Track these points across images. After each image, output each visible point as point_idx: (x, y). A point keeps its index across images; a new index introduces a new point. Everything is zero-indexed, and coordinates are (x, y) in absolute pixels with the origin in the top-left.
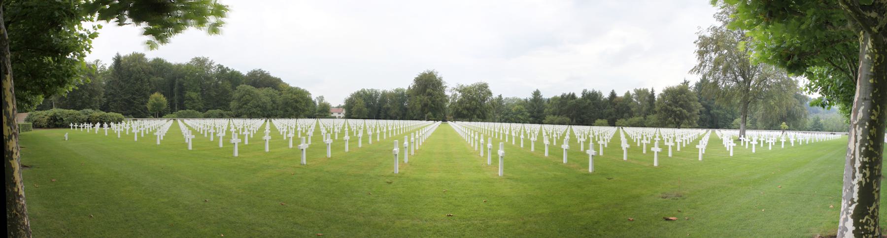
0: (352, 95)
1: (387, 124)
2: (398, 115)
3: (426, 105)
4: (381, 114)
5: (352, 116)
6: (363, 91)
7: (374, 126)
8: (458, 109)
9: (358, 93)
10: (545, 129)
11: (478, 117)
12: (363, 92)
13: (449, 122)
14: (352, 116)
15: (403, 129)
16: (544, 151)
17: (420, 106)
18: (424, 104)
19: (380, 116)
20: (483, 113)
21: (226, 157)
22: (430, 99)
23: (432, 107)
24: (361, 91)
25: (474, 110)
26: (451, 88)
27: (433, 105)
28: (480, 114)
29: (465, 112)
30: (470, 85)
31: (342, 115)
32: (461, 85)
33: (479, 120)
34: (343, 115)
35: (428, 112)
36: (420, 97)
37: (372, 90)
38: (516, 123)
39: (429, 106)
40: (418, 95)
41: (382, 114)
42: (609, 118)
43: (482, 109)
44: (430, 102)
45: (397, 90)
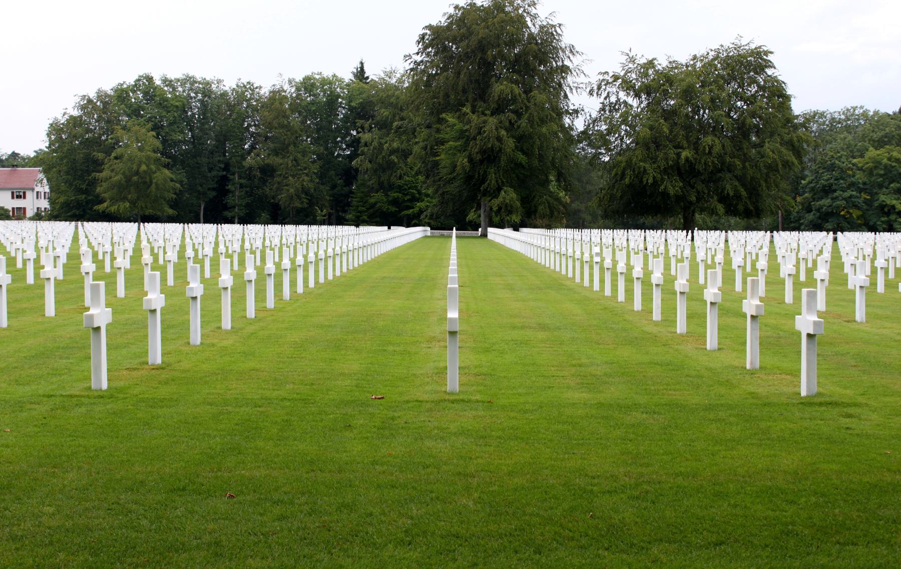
0: (88, 105)
1: (727, 252)
2: (313, 200)
3: (490, 156)
4: (230, 200)
5: (101, 207)
6: (146, 84)
7: (869, 251)
8: (640, 175)
9: (122, 94)
10: (90, 245)
11: (731, 211)
12: (146, 94)
13: (494, 233)
14: (101, 207)
15: (306, 270)
16: (796, 374)
17: (462, 161)
18: (483, 152)
19: (226, 207)
20: (754, 192)
21: (88, 422)
22: (511, 127)
23: (520, 165)
24: (135, 87)
25: (714, 176)
26: (595, 79)
27: (521, 158)
28: (738, 196)
29: (673, 187)
30: (683, 58)
31: (32, 203)
32: (643, 61)
33: (733, 220)
34: (44, 204)
35: (499, 189)
36: (462, 117)
37: (189, 80)
38: (874, 229)
39: (503, 159)
40: (446, 107)
41: (236, 198)
42: (147, 127)
43: (750, 172)
44: (510, 143)
45: (308, 85)
